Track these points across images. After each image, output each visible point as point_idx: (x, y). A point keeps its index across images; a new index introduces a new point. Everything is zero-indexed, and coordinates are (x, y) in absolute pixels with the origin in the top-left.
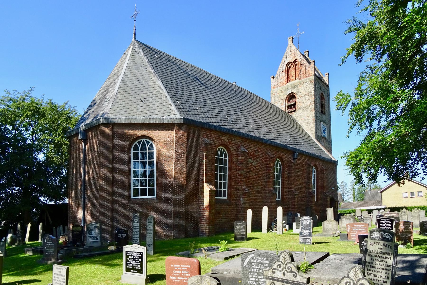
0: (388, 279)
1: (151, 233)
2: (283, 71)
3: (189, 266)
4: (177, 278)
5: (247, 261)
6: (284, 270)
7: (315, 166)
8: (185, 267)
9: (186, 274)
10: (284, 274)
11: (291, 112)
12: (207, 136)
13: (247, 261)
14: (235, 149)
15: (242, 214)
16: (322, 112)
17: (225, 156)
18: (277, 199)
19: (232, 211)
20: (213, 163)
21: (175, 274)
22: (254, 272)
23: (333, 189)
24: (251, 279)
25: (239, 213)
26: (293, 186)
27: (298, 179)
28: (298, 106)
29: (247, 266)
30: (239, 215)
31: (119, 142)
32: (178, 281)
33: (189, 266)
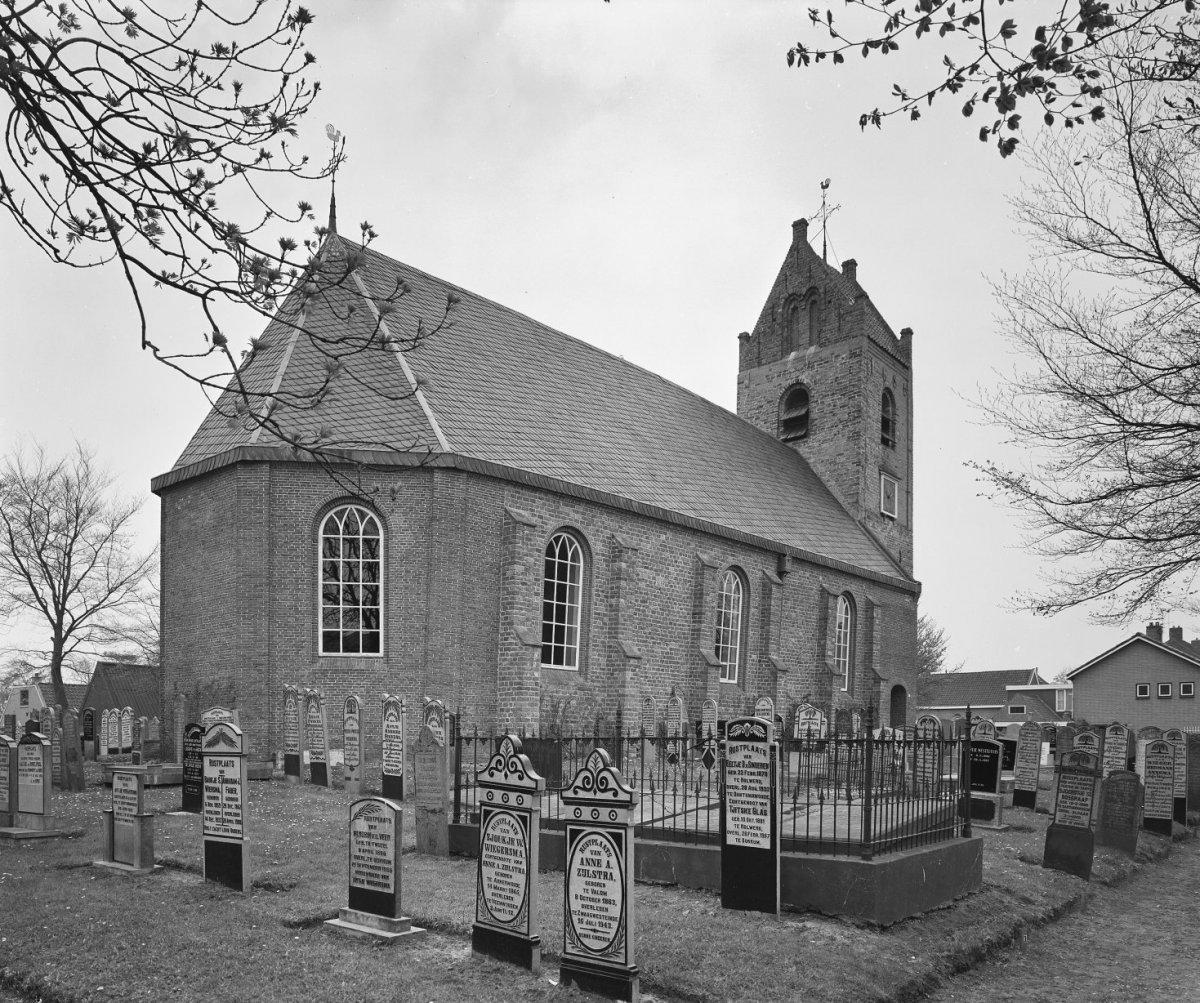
0: (766, 815)
1: (355, 739)
7: (848, 595)
10: (506, 776)
17: (575, 558)
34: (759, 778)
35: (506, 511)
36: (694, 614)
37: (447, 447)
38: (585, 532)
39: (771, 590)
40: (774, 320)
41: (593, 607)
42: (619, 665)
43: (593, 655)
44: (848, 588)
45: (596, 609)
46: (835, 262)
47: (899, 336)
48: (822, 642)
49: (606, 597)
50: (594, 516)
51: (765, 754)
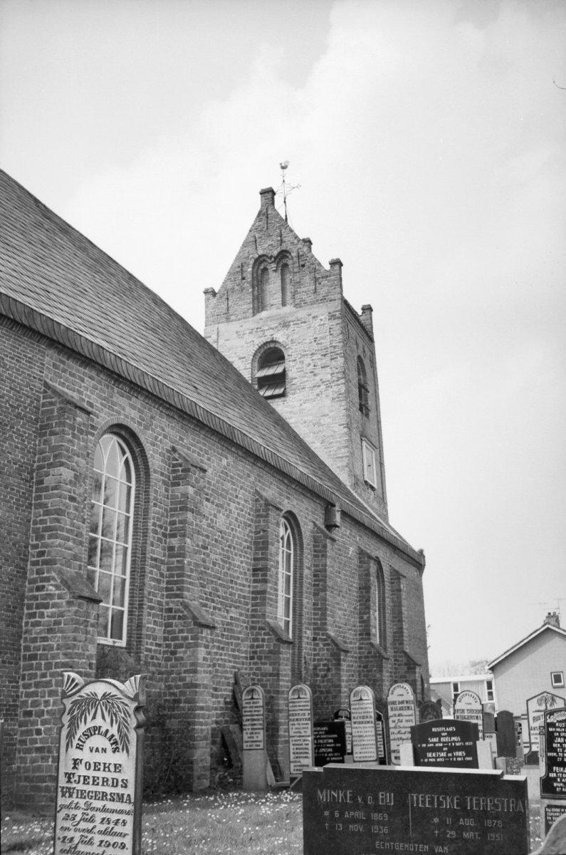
28: (294, 382)
35: (46, 384)
36: (254, 570)
38: (142, 438)
39: (325, 546)
40: (243, 279)
41: (149, 548)
42: (186, 638)
43: (149, 623)
45: (153, 552)
47: (360, 312)
48: (365, 617)
49: (165, 535)
50: (152, 417)
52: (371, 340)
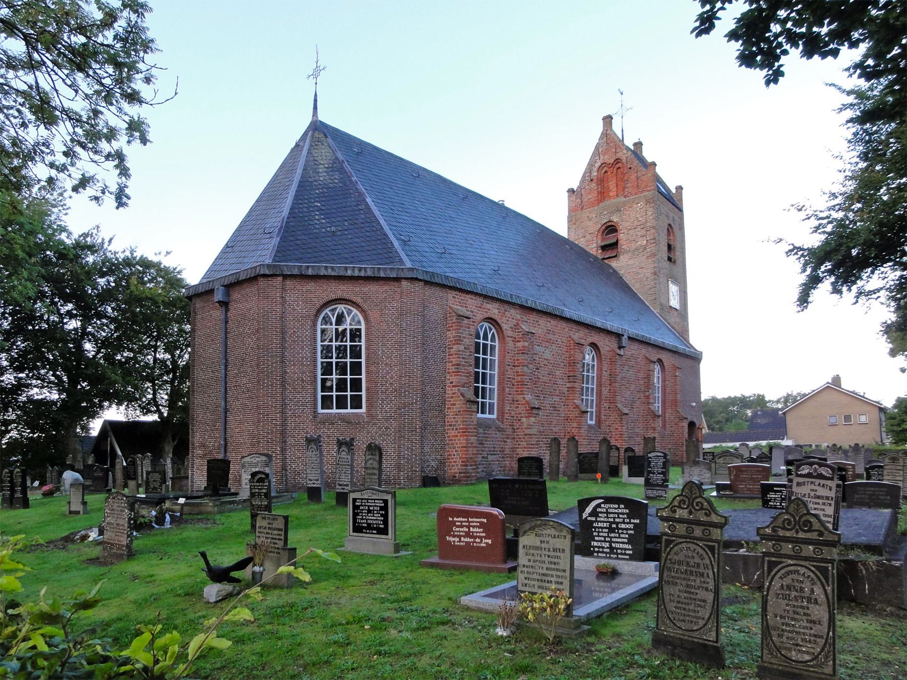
1: (375, 474)
2: (592, 180)
3: (485, 520)
4: (460, 539)
5: (589, 510)
6: (691, 507)
8: (476, 522)
9: (477, 532)
11: (609, 258)
12: (460, 302)
13: (589, 510)
14: (511, 328)
15: (524, 448)
16: (670, 259)
17: (493, 340)
18: (590, 422)
19: (506, 442)
20: (471, 352)
21: (456, 533)
22: (602, 528)
23: (694, 404)
24: (596, 538)
25: (519, 445)
26: (618, 398)
27: (628, 386)
29: (589, 518)
30: (518, 448)
31: (294, 310)
32: (462, 544)
33: (485, 520)
34: (823, 507)
37: (409, 265)
38: (500, 322)
44: (660, 357)
46: (629, 142)
50: (506, 311)
51: (830, 489)
52: (680, 210)
